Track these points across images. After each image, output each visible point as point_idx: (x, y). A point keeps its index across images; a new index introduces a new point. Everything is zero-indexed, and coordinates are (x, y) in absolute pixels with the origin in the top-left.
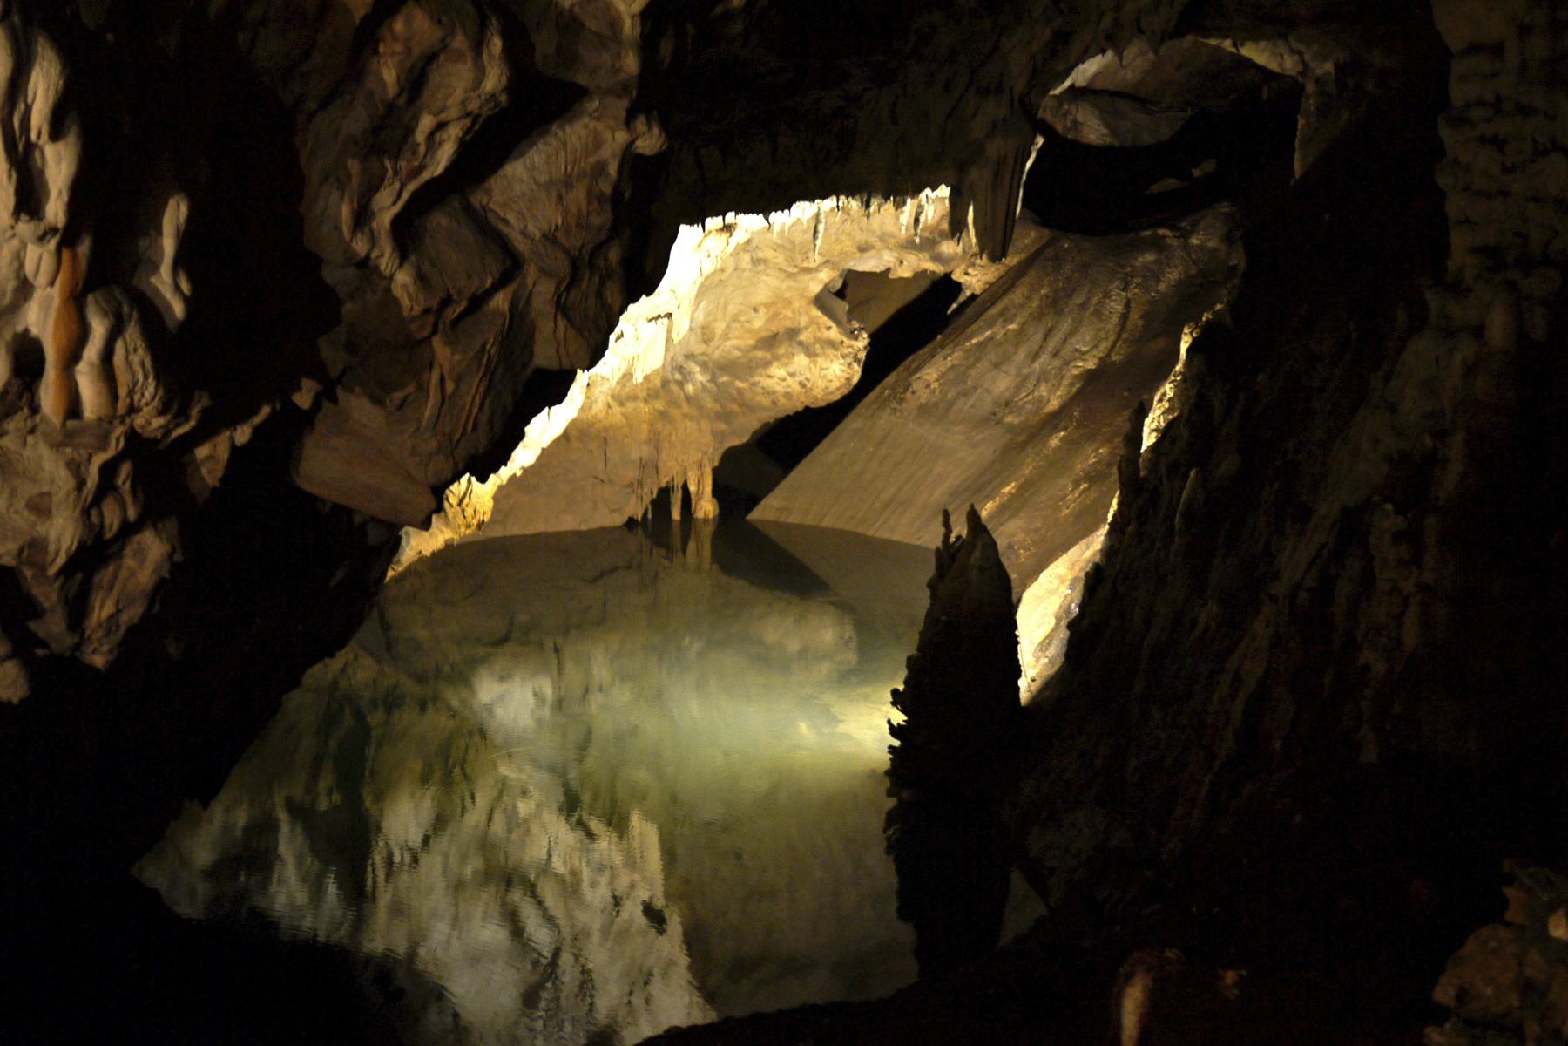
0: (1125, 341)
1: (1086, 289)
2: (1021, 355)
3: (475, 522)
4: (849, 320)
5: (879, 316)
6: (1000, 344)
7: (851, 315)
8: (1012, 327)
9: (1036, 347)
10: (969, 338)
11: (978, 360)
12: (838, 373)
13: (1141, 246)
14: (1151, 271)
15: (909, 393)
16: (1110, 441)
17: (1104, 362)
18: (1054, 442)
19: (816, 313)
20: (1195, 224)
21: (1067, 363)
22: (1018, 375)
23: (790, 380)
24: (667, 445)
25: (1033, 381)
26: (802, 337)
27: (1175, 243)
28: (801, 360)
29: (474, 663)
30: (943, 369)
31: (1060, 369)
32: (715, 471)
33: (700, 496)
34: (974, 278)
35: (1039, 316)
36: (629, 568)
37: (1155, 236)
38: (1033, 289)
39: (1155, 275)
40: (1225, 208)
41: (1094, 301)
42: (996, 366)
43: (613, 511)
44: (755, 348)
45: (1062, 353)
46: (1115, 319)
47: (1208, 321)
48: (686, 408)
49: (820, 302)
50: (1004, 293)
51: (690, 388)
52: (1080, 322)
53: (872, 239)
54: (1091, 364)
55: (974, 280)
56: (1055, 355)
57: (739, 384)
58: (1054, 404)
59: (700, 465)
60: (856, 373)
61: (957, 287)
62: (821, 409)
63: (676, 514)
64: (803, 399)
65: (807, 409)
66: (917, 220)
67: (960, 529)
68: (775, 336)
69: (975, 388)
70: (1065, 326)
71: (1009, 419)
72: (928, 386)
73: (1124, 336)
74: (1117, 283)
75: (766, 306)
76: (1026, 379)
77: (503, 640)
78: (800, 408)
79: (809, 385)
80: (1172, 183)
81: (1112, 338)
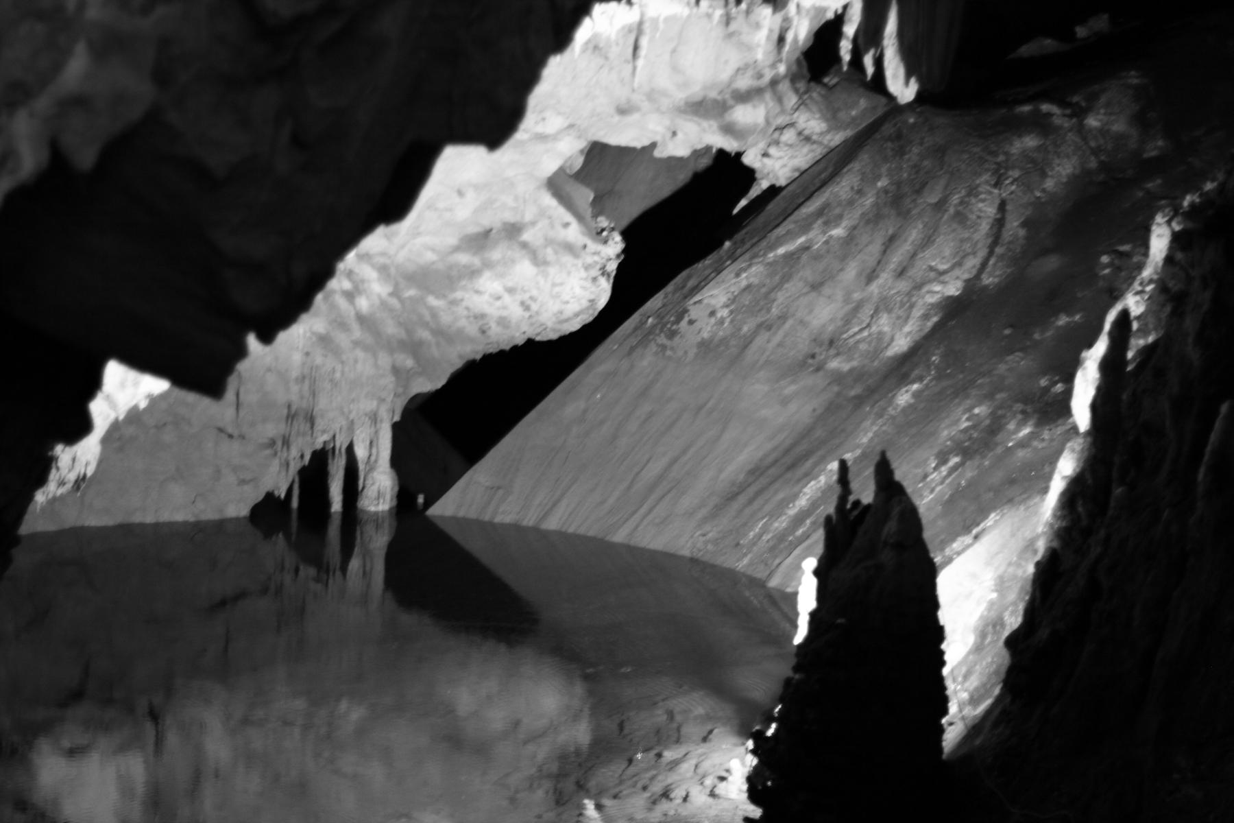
0: (1001, 257)
1: (943, 182)
2: (851, 272)
3: (72, 477)
4: (595, 216)
5: (633, 208)
6: (817, 257)
7: (599, 205)
8: (838, 232)
9: (872, 262)
10: (772, 247)
11: (786, 278)
12: (578, 291)
13: (1018, 126)
14: (1033, 161)
15: (684, 323)
16: (990, 396)
17: (971, 286)
18: (904, 398)
19: (549, 201)
20: (1093, 98)
21: (918, 287)
22: (847, 300)
23: (507, 299)
24: (328, 386)
25: (868, 310)
26: (526, 236)
27: (1067, 124)
28: (524, 269)
29: (34, 731)
30: (735, 289)
31: (909, 294)
32: (396, 427)
33: (371, 465)
34: (775, 164)
35: (873, 219)
36: (265, 591)
37: (1037, 112)
38: (869, 178)
39: (1037, 166)
40: (1134, 78)
41: (955, 199)
42: (816, 287)
43: (243, 482)
44: (457, 249)
45: (911, 273)
46: (985, 227)
47: (1192, 205)
48: (357, 332)
49: (555, 185)
50: (824, 184)
51: (363, 304)
52: (936, 229)
53: (637, 98)
54: (953, 289)
55: (778, 165)
56: (901, 273)
57: (432, 301)
58: (901, 344)
59: (374, 418)
60: (603, 293)
61: (749, 175)
62: (550, 342)
63: (337, 505)
64: (524, 328)
65: (530, 342)
66: (781, 40)
67: (865, 492)
68: (487, 233)
69: (783, 318)
70: (914, 234)
71: (834, 364)
72: (712, 313)
73: (999, 250)
74: (986, 177)
75: (477, 187)
76: (858, 307)
77: (77, 695)
78: (520, 340)
79: (534, 307)
80: (1048, 44)
81: (982, 253)
